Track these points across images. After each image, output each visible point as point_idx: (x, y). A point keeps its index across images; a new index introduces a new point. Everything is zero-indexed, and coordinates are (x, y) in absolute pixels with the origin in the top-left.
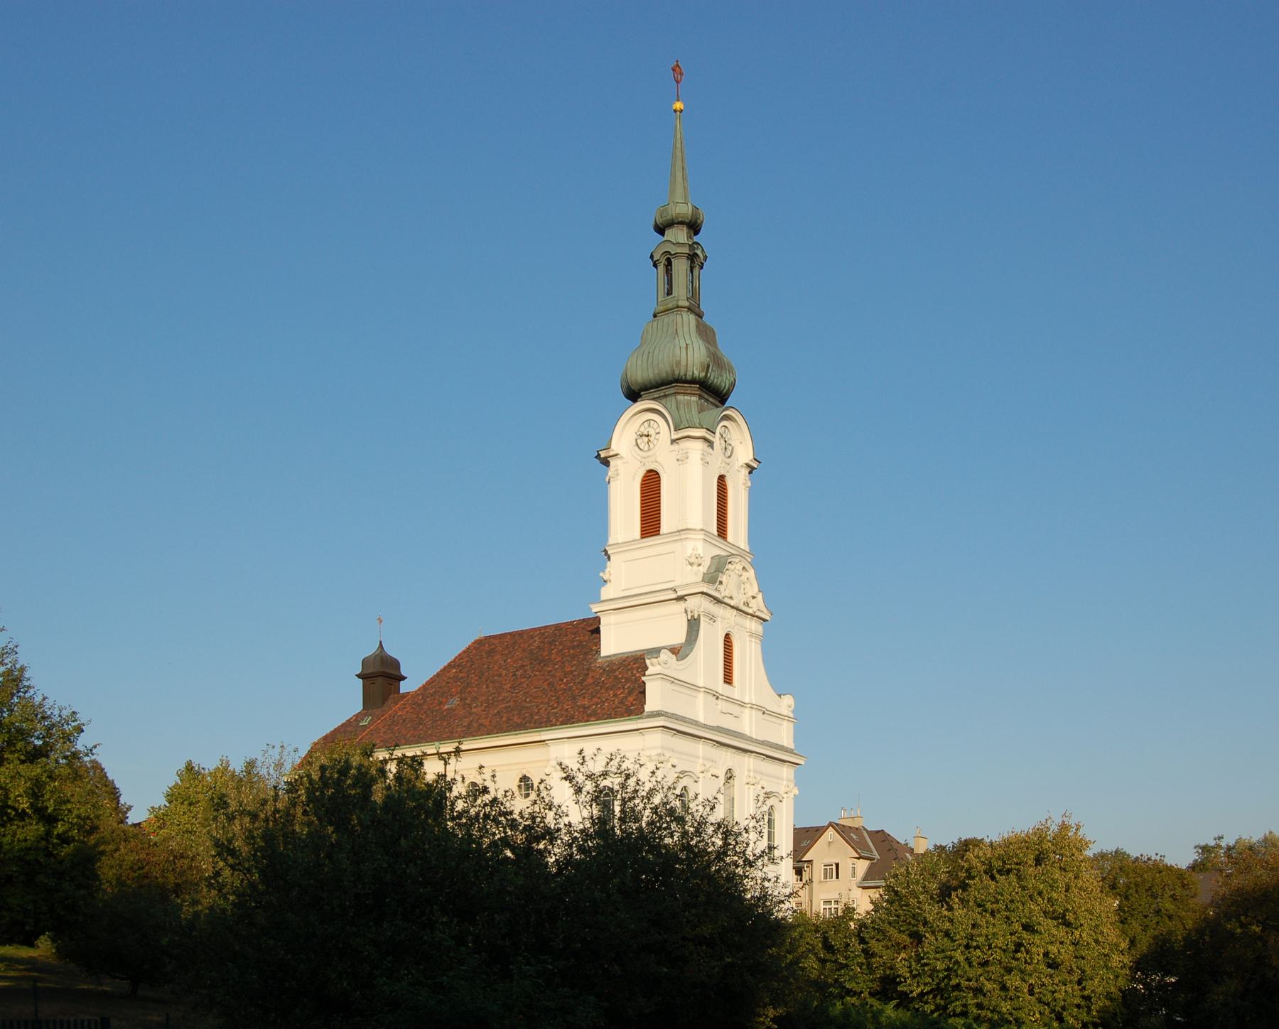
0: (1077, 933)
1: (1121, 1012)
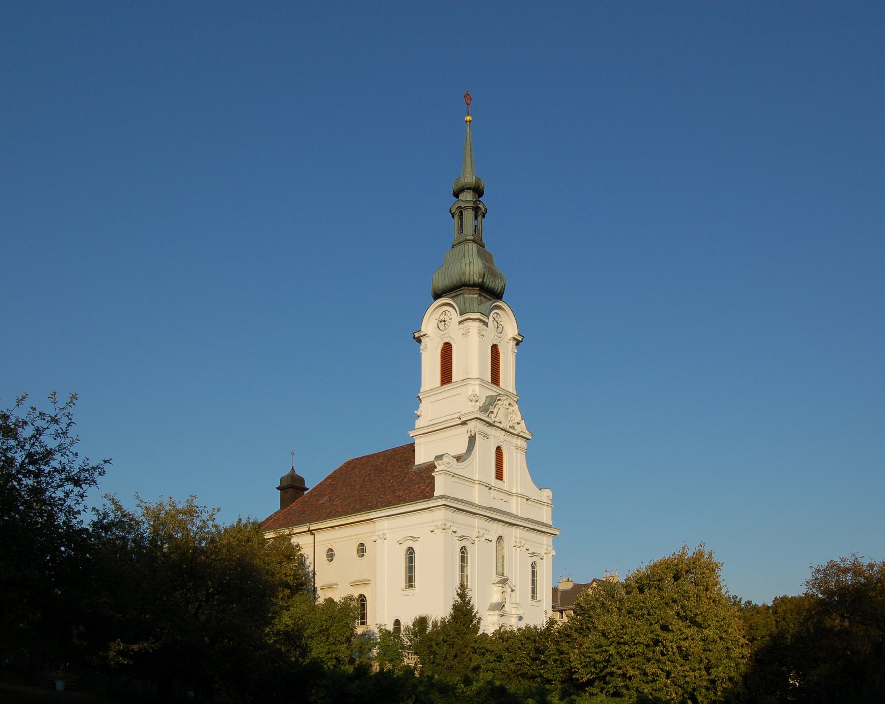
0: (705, 632)
1: (744, 693)
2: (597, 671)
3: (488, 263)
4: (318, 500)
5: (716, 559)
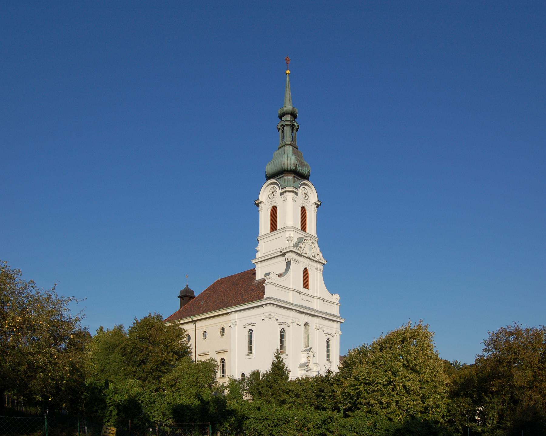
3: (299, 158)
4: (199, 303)
5: (429, 330)
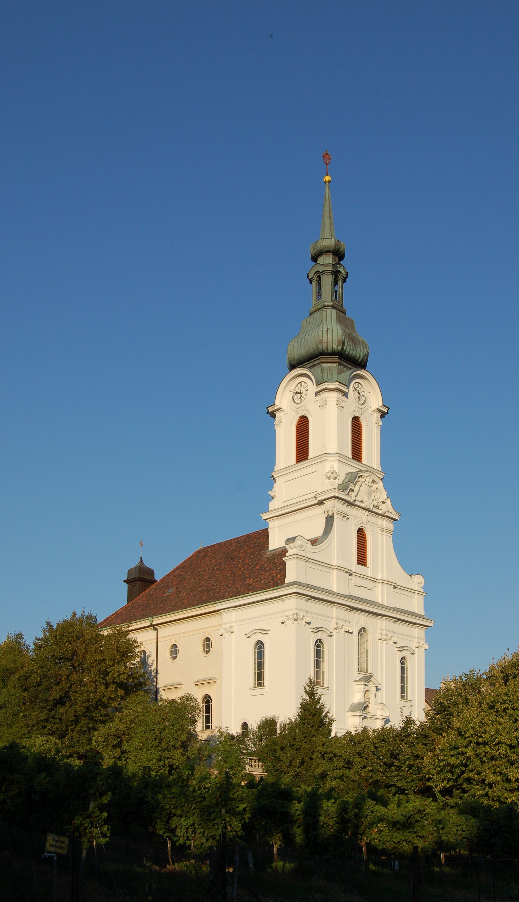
2: (454, 778)
4: (164, 592)
